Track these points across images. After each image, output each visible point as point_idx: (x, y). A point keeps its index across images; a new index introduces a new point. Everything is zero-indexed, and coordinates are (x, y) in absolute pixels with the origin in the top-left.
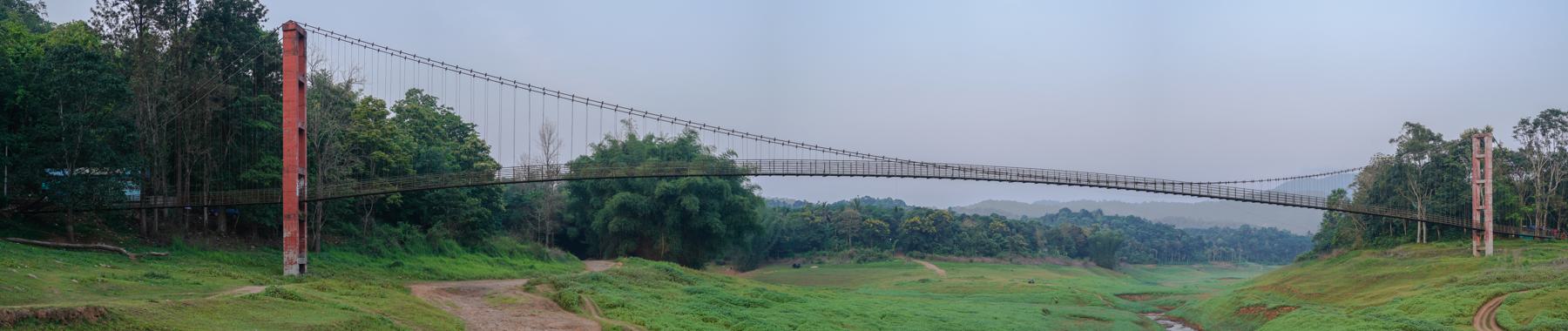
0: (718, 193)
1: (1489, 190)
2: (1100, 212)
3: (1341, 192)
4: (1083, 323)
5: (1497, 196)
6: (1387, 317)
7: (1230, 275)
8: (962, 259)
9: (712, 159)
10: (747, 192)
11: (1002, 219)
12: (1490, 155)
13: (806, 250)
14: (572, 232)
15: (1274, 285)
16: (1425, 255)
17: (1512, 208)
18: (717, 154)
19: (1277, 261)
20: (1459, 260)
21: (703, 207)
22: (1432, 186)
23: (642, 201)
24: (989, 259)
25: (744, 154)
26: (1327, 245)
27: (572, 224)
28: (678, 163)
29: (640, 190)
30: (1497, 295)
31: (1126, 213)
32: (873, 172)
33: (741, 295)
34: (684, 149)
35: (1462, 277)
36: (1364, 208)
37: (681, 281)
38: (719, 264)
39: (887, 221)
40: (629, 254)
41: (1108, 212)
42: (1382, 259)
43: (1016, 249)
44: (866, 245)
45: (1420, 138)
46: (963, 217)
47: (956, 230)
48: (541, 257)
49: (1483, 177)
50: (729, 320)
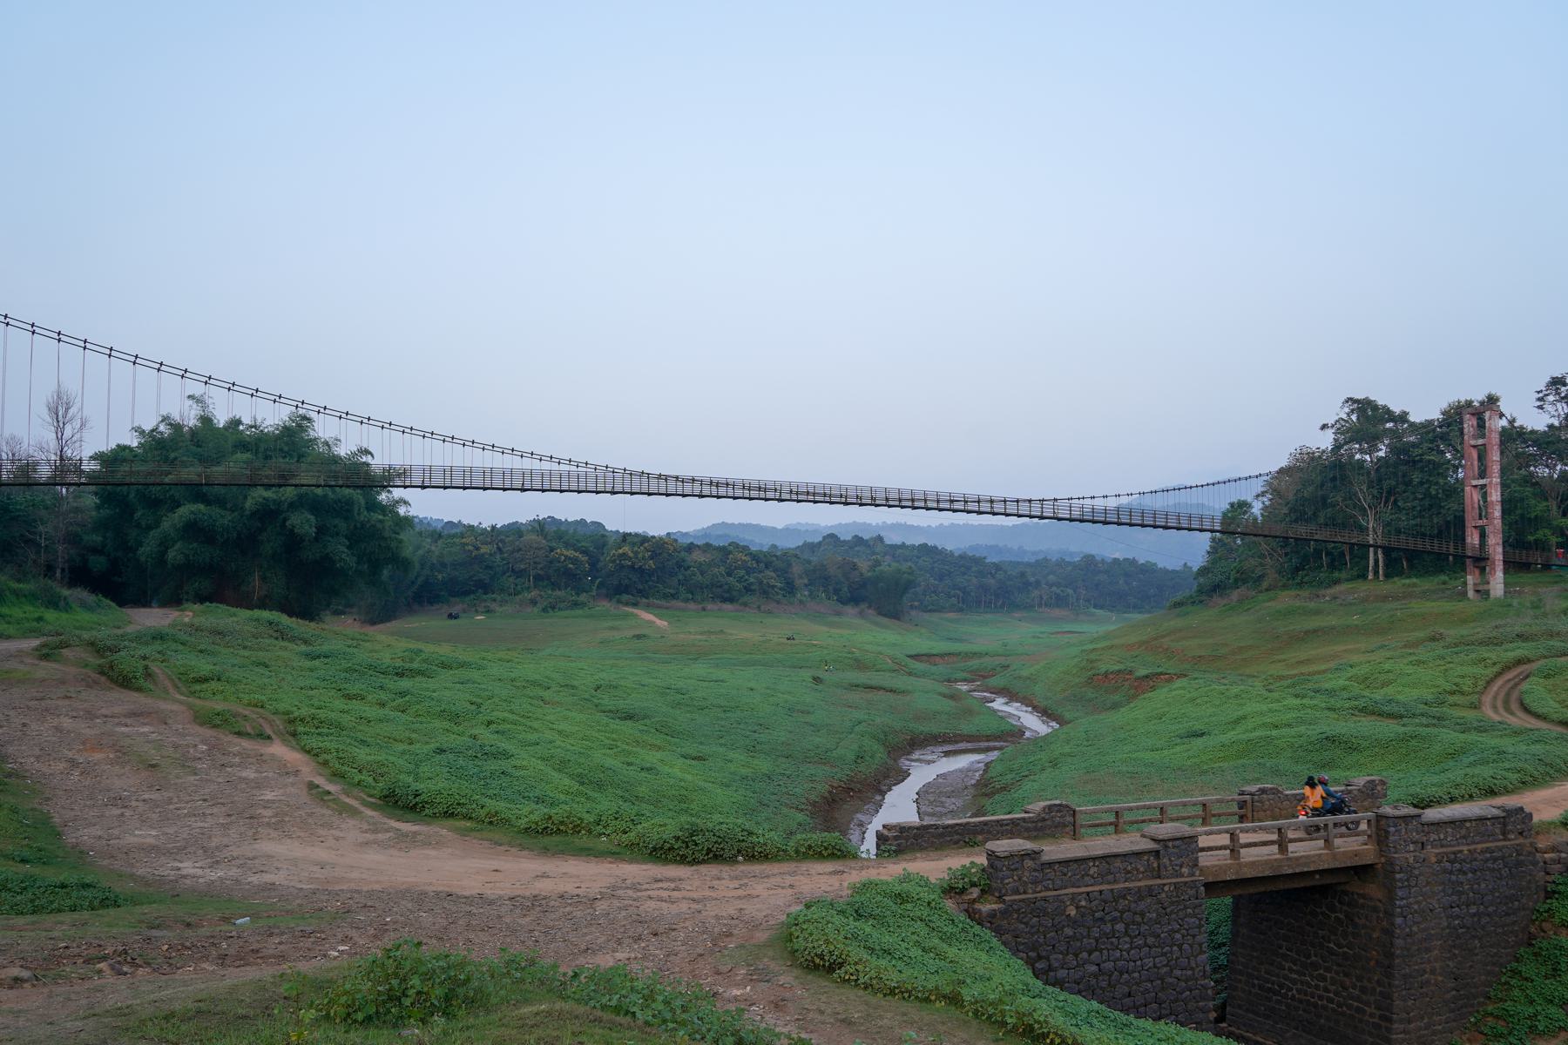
0: (344, 509)
1: (1495, 496)
2: (880, 538)
3: (1242, 506)
4: (870, 695)
5: (1508, 505)
6: (1331, 693)
7: (1068, 627)
8: (692, 605)
9: (336, 460)
10: (389, 509)
11: (746, 548)
12: (1495, 438)
13: (466, 593)
14: (98, 563)
15: (1141, 643)
16: (1385, 598)
17: (1537, 522)
18: (342, 451)
19: (1137, 608)
20: (1447, 606)
21: (321, 530)
22: (1390, 492)
23: (223, 518)
24: (728, 606)
25: (385, 453)
26: (1214, 584)
27: (96, 551)
28: (279, 462)
29: (220, 502)
30: (1519, 662)
31: (917, 541)
32: (591, 487)
33: (386, 659)
34: (293, 440)
35: (1453, 633)
36: (1279, 530)
37: (293, 639)
38: (337, 613)
39: (585, 552)
40: (201, 599)
41: (892, 539)
42: (1312, 605)
43: (766, 592)
44: (555, 586)
45: (1368, 419)
46: (691, 548)
47: (680, 565)
48: (54, 603)
49: (1482, 475)
50: (383, 696)
